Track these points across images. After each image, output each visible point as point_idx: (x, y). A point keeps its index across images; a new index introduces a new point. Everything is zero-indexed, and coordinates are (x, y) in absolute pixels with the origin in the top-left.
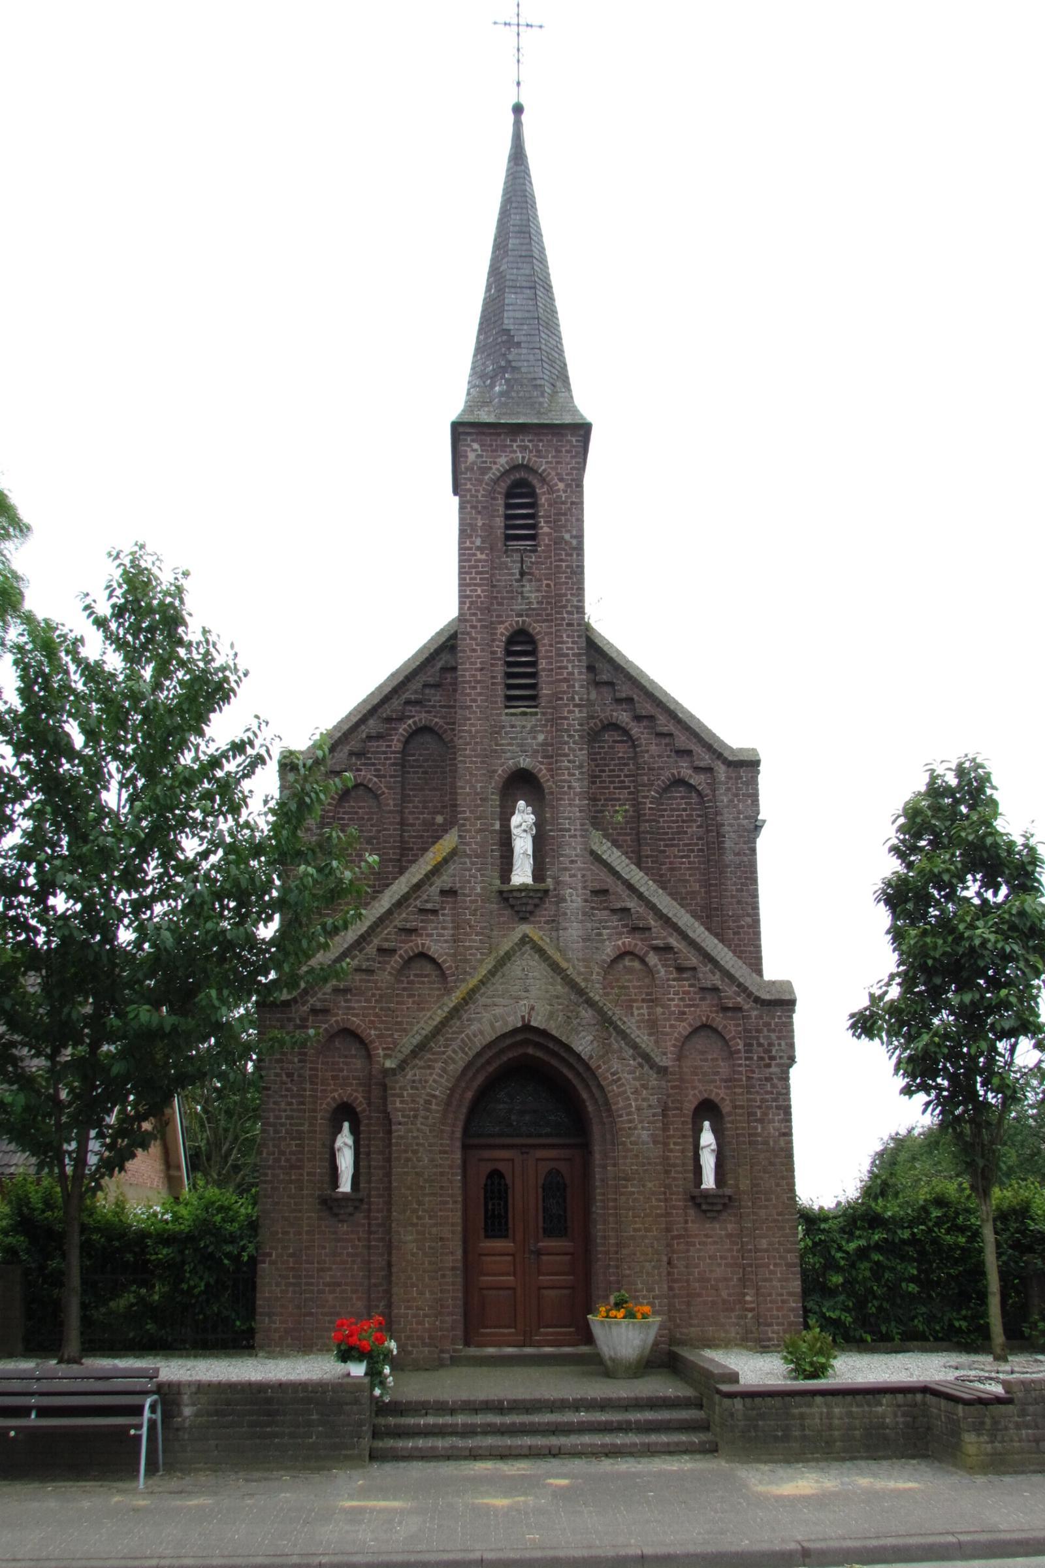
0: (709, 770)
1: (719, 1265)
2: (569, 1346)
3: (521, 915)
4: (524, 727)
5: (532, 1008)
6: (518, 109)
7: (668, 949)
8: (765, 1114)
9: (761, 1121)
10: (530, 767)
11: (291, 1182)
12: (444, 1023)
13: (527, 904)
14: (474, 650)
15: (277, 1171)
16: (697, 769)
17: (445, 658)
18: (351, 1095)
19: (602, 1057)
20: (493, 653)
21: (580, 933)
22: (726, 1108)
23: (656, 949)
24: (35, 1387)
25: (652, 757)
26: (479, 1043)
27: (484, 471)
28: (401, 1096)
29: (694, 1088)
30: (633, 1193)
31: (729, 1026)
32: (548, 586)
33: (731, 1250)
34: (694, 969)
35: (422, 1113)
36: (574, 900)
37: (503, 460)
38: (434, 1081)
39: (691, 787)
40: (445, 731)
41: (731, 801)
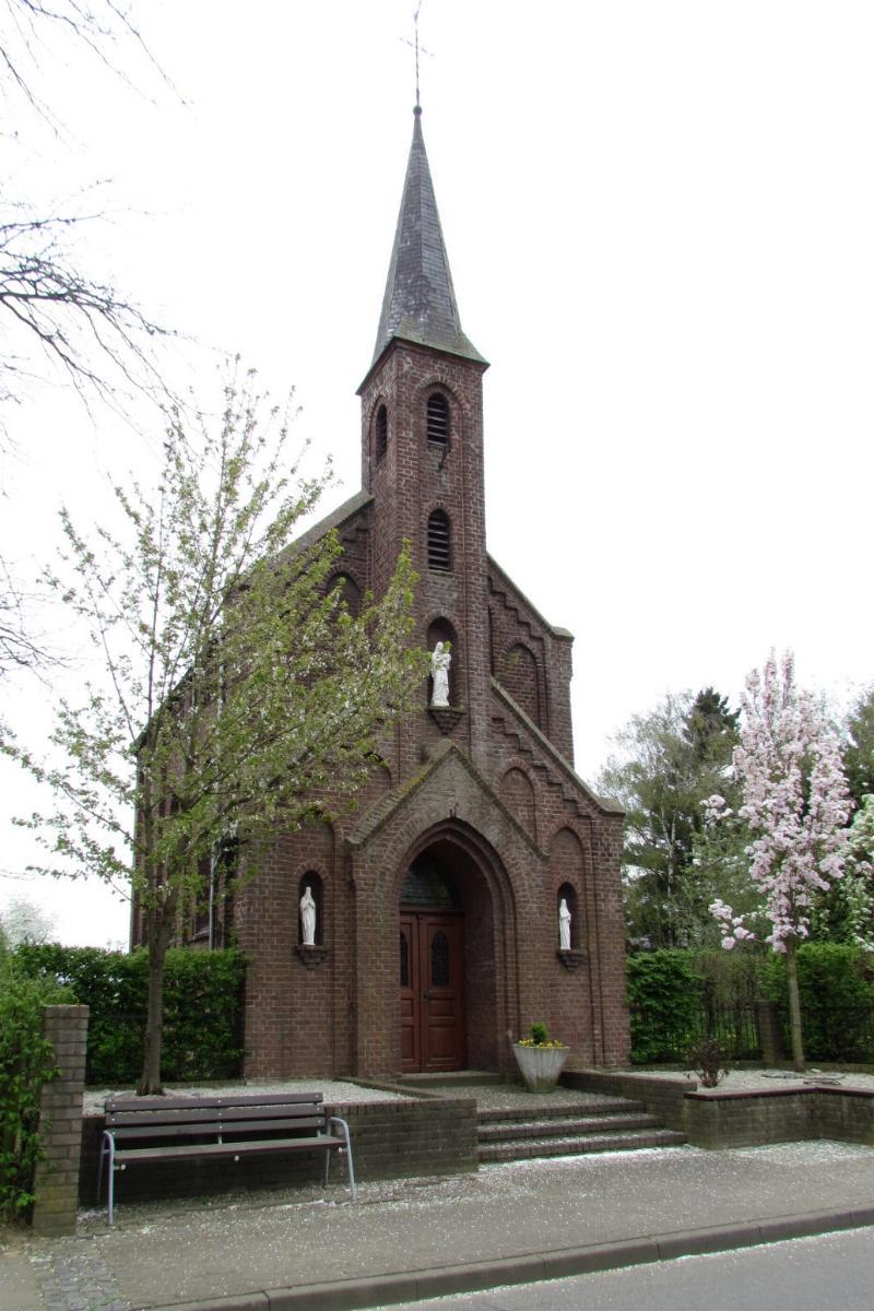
0: (540, 639)
1: (576, 1007)
2: (452, 1071)
3: (444, 730)
4: (443, 585)
5: (457, 805)
6: (418, 111)
7: (543, 768)
8: (606, 896)
9: (604, 900)
10: (448, 617)
11: (273, 935)
12: (395, 811)
13: (448, 723)
14: (409, 519)
15: (269, 931)
16: (533, 638)
17: (359, 522)
18: (316, 864)
19: (504, 846)
20: (421, 523)
21: (486, 749)
22: (579, 890)
23: (536, 767)
24: (220, 1115)
25: (502, 623)
26: (420, 828)
27: (415, 380)
28: (363, 867)
29: (558, 874)
30: (526, 951)
31: (581, 829)
32: (458, 480)
33: (583, 996)
34: (560, 784)
35: (379, 882)
36: (481, 724)
37: (428, 376)
38: (388, 857)
39: (528, 650)
40: (358, 579)
41: (555, 664)
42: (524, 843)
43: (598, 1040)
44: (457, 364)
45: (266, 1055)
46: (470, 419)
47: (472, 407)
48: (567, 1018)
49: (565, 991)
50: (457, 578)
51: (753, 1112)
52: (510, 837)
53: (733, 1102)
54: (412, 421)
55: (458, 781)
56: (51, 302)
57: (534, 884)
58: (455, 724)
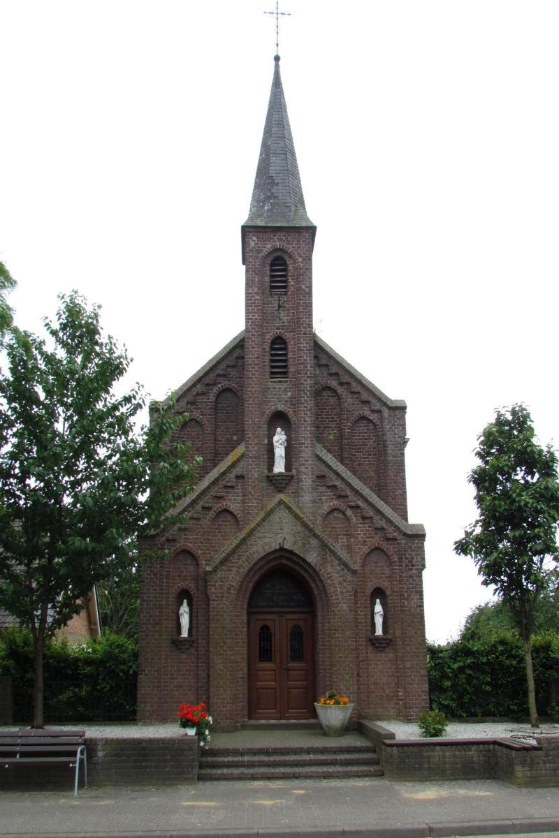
0: (379, 411)
3: (279, 489)
4: (280, 388)
5: (285, 539)
6: (277, 59)
7: (357, 507)
8: (409, 595)
9: (407, 599)
11: (156, 631)
12: (237, 547)
14: (253, 348)
15: (148, 626)
16: (373, 411)
20: (264, 349)
21: (310, 498)
22: (388, 592)
23: (351, 507)
24: (19, 741)
26: (256, 557)
27: (259, 252)
29: (371, 581)
31: (390, 548)
34: (371, 518)
35: (226, 595)
36: (307, 481)
37: (269, 246)
40: (238, 391)
42: (337, 562)
43: (401, 700)
44: (292, 232)
45: (151, 707)
46: (302, 269)
47: (304, 260)
48: (376, 684)
49: (377, 665)
50: (291, 382)
51: (429, 757)
52: (326, 558)
53: (426, 747)
54: (257, 280)
55: (286, 523)
56: (237, 204)
57: (345, 590)
58: (287, 484)
